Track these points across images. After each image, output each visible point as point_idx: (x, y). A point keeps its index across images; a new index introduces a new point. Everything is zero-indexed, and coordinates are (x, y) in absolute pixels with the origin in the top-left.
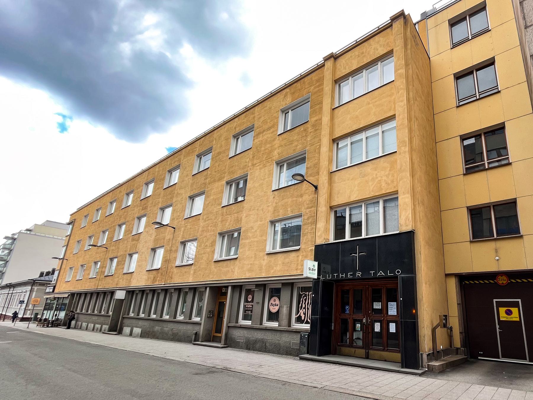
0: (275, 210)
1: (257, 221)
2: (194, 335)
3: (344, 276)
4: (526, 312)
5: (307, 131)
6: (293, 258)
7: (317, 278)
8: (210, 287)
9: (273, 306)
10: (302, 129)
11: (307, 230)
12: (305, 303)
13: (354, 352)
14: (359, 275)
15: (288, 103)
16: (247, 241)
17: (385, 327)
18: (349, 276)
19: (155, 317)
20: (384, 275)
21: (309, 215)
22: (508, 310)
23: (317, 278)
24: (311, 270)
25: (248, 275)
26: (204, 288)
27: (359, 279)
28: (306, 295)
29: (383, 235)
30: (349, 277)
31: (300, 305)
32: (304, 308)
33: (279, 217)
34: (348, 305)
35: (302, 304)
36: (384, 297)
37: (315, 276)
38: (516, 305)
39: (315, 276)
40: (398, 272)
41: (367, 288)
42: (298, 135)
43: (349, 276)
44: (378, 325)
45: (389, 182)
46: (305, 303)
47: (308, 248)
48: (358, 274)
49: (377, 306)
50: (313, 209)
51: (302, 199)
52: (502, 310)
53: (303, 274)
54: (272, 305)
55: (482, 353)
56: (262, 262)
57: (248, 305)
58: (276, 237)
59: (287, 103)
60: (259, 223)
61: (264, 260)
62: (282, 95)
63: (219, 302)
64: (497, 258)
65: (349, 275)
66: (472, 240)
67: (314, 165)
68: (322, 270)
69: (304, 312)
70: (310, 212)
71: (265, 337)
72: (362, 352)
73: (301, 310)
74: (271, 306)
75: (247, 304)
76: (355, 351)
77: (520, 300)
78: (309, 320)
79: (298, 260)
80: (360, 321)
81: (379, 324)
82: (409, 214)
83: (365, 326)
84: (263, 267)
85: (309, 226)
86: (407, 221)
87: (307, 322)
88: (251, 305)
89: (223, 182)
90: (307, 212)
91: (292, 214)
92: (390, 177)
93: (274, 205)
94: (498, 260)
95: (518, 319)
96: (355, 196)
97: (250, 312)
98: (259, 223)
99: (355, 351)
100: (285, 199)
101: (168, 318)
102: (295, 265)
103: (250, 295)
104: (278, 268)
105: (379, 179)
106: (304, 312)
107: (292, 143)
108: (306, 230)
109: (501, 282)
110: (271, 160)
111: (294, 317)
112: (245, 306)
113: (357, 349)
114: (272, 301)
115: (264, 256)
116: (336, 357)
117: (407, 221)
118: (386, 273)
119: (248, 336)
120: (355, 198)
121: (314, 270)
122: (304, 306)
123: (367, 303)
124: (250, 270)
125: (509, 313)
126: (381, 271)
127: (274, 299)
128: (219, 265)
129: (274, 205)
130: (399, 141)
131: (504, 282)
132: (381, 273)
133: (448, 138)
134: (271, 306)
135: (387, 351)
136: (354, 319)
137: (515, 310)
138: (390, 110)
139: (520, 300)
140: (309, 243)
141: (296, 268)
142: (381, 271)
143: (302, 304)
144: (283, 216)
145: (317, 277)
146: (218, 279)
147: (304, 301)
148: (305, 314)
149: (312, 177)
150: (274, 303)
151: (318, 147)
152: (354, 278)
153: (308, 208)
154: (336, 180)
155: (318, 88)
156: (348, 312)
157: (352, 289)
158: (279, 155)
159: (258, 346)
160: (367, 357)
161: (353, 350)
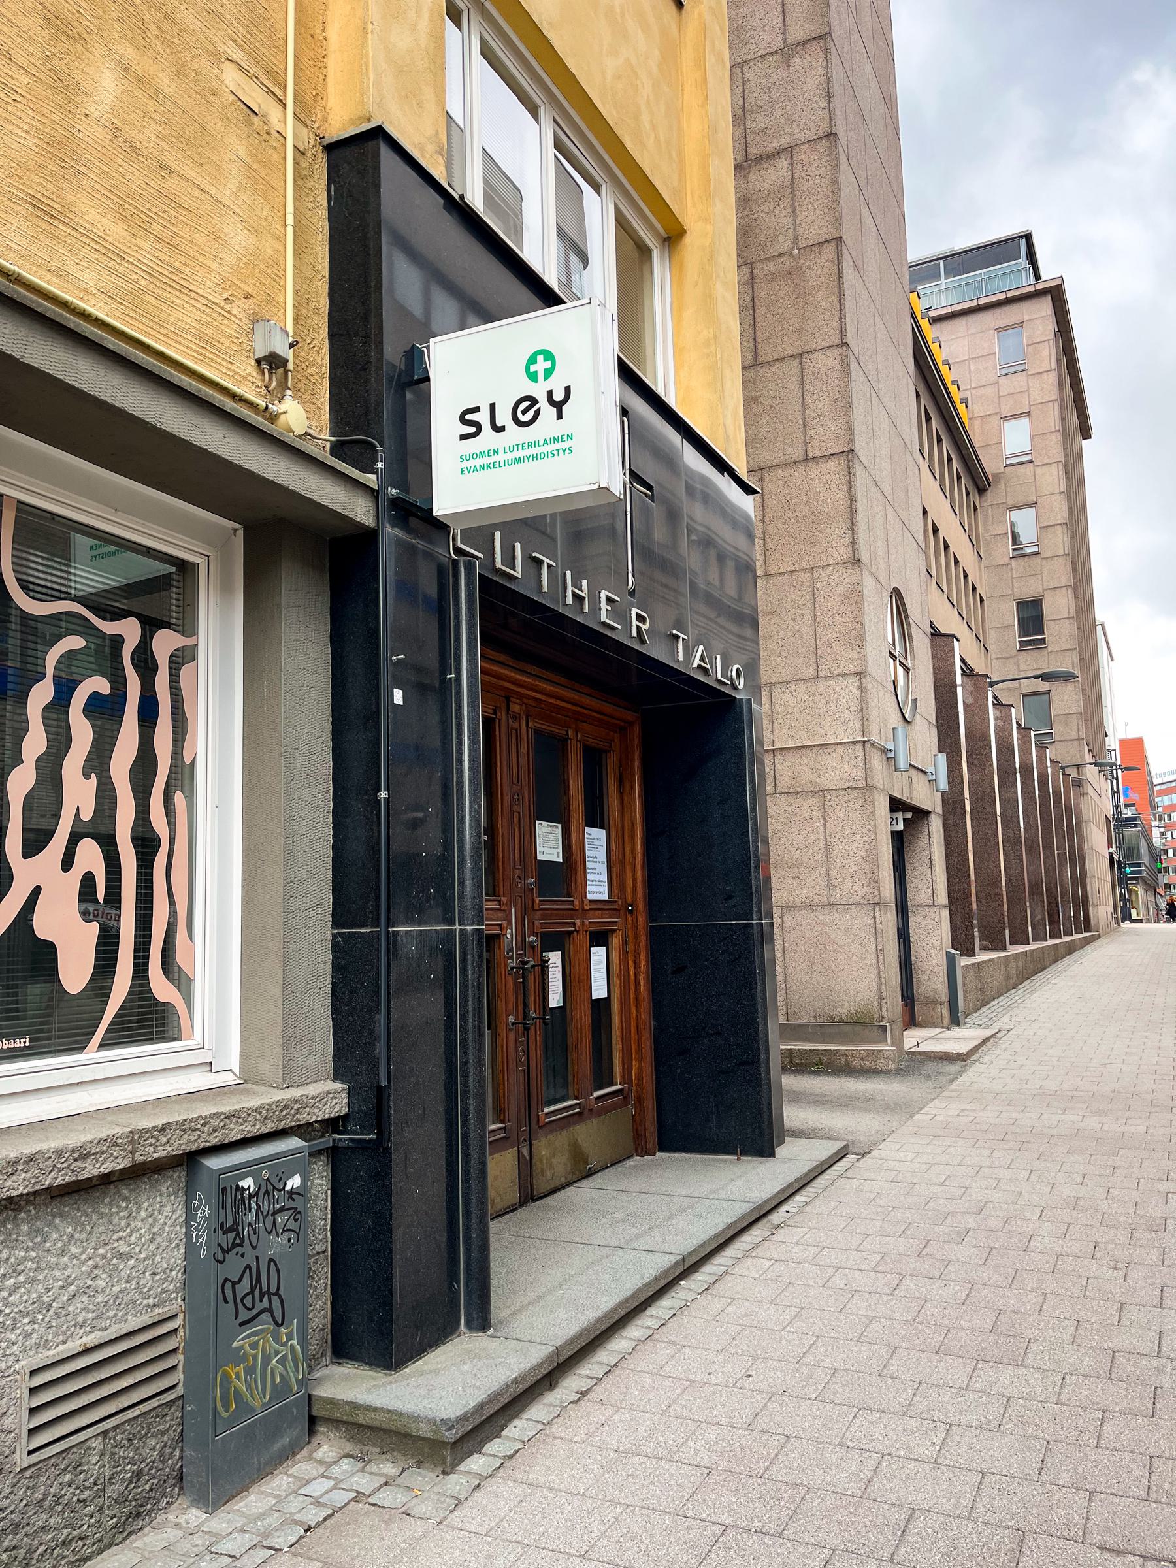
12: (98, 762)
46: (98, 762)
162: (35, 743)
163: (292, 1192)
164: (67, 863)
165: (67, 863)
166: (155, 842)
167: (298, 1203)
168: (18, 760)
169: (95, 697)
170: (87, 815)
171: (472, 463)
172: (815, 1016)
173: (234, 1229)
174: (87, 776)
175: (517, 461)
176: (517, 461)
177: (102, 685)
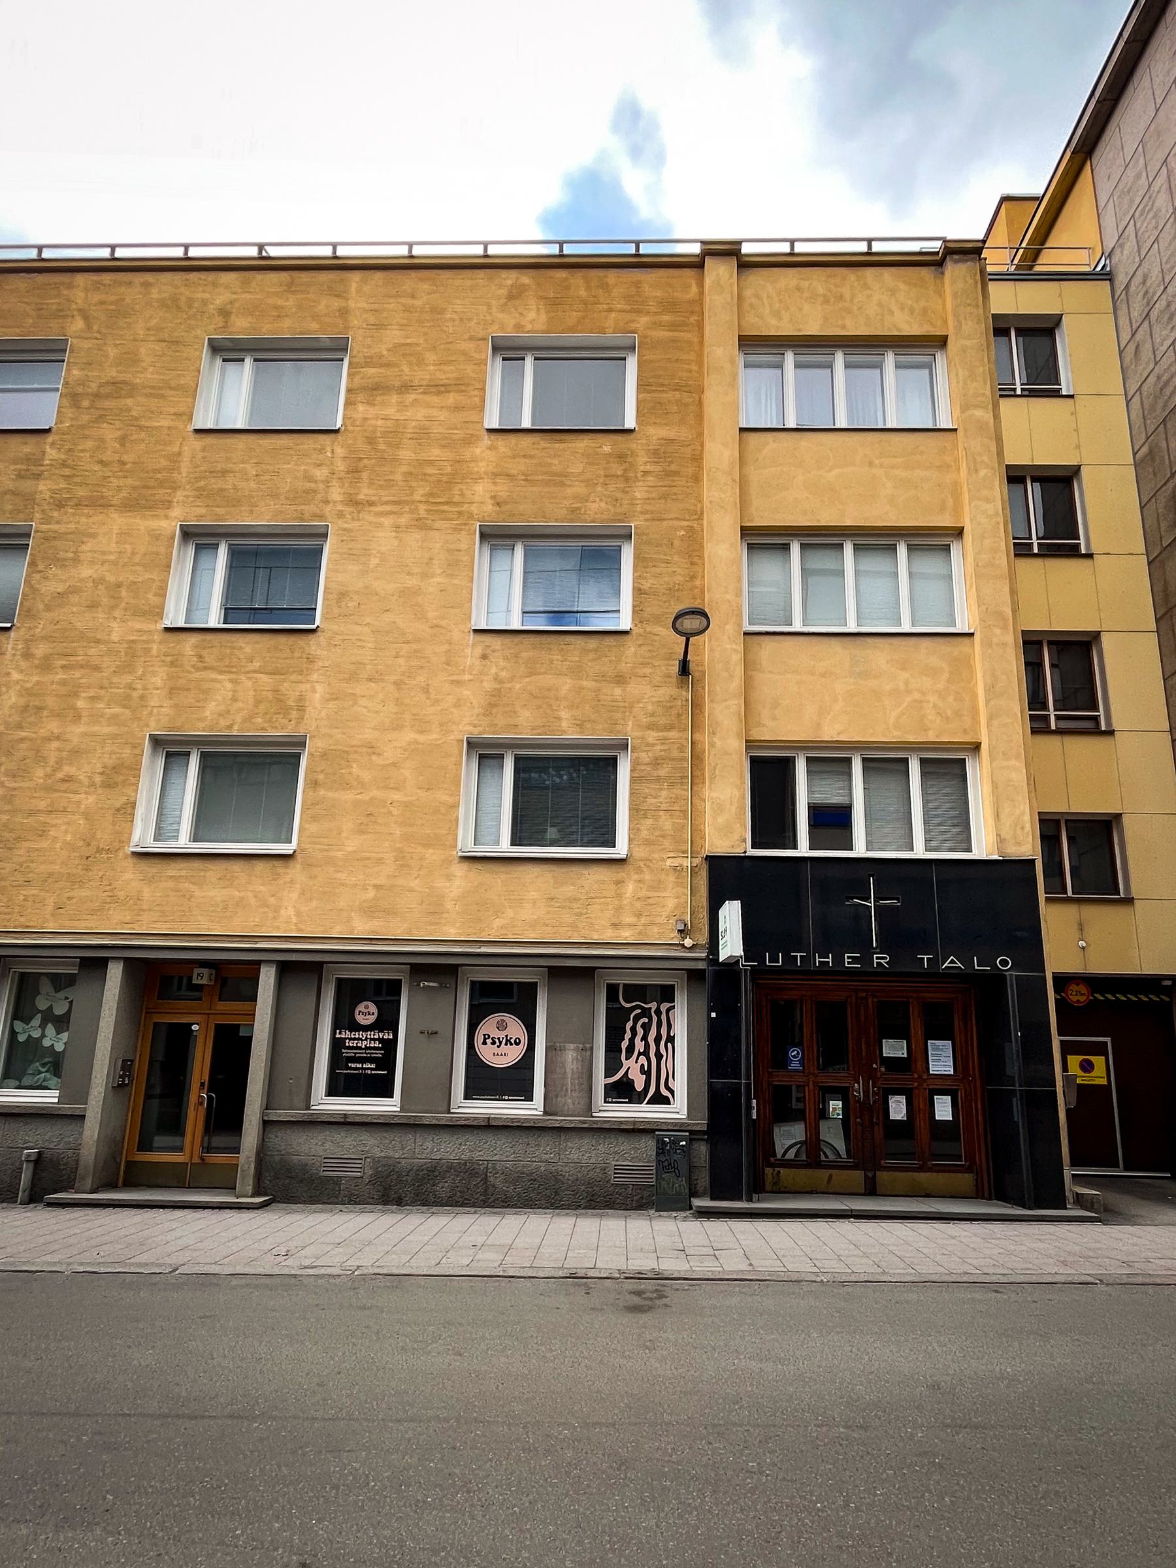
0: (495, 702)
1: (397, 727)
2: (31, 1165)
4: (1121, 1068)
5: (631, 465)
6: (595, 886)
8: (127, 961)
9: (493, 1043)
11: (653, 801)
12: (645, 1038)
13: (825, 1182)
15: (529, 327)
16: (348, 796)
17: (920, 1107)
18: (849, 963)
19: (56, 1100)
22: (1084, 1060)
25: (362, 927)
26: (73, 965)
27: (881, 973)
28: (646, 1013)
29: (806, 855)
32: (640, 1054)
33: (516, 733)
34: (800, 1044)
35: (632, 1041)
36: (916, 1026)
38: (1100, 1050)
40: (1004, 963)
42: (589, 464)
43: (849, 963)
44: (899, 1101)
45: (949, 713)
46: (645, 1038)
47: (664, 860)
48: (877, 958)
49: (894, 1049)
51: (624, 690)
52: (1074, 1061)
54: (489, 1041)
56: (441, 884)
57: (359, 1039)
58: (173, 793)
59: (523, 326)
60: (409, 736)
61: (449, 877)
62: (501, 286)
63: (155, 1024)
64: (1082, 943)
65: (846, 960)
70: (663, 740)
71: (478, 1155)
72: (858, 1176)
74: (484, 1043)
75: (346, 1034)
76: (831, 1176)
77: (1108, 1040)
79: (619, 896)
80: (843, 1093)
82: (1023, 814)
84: (449, 905)
86: (1019, 832)
88: (375, 1040)
89: (164, 524)
90: (650, 740)
91: (581, 733)
92: (951, 699)
93: (488, 685)
94: (1083, 948)
95: (1104, 1082)
96: (838, 727)
97: (373, 1066)
98: (409, 736)
99: (831, 1176)
100: (545, 673)
101: (56, 1100)
102: (609, 913)
103: (366, 1003)
104: (527, 913)
105: (917, 696)
106: (642, 1065)
107: (562, 484)
108: (651, 800)
109: (1074, 999)
111: (600, 1081)
112: (337, 1045)
113: (835, 1172)
114: (488, 1026)
115: (447, 862)
116: (117, 1192)
117: (1019, 832)
119: (390, 1153)
120: (839, 734)
122: (639, 1046)
124: (370, 911)
125: (1087, 1067)
128: (171, 873)
129: (485, 684)
130: (983, 608)
131: (1082, 999)
132: (951, 962)
134: (484, 1043)
135: (930, 1170)
136: (821, 1088)
137: (1098, 1061)
138: (943, 509)
139: (1108, 1040)
140: (667, 843)
141: (615, 920)
143: (632, 1041)
144: (535, 732)
146: (323, 933)
148: (648, 1074)
149: (662, 626)
150: (496, 1034)
151: (683, 532)
153: (651, 727)
154: (764, 663)
155: (671, 334)
156: (795, 1065)
159: (443, 1188)
160: (871, 1191)
161: (824, 1174)
162: (628, 1035)
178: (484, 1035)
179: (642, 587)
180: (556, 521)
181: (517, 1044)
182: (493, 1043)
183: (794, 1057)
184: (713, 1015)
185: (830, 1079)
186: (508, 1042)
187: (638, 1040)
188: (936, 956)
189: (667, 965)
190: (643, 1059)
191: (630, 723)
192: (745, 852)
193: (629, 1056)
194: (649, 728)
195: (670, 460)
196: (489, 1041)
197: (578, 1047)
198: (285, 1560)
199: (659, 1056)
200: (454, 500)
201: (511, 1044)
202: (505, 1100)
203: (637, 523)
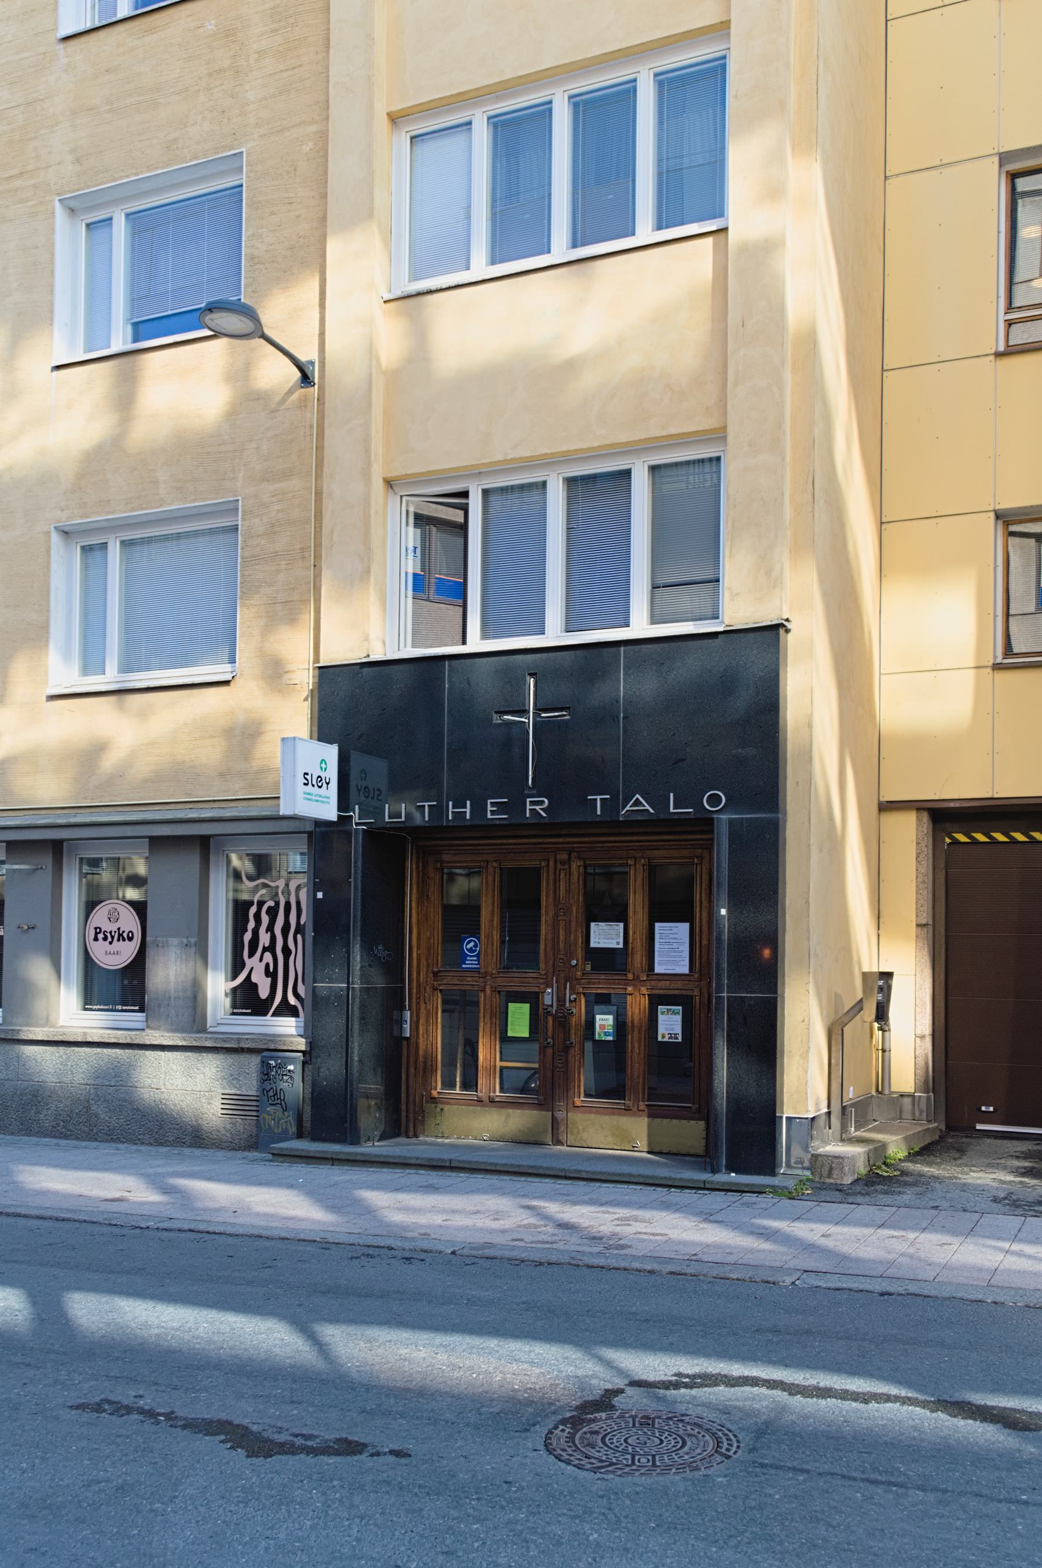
3: (468, 810)
7: (335, 818)
9: (105, 939)
10: (210, 27)
12: (270, 928)
14: (537, 808)
20: (652, 811)
21: (278, 511)
23: (335, 818)
24: (314, 783)
27: (539, 827)
30: (489, 816)
31: (248, 936)
32: (265, 949)
36: (637, 903)
37: (330, 812)
39: (330, 812)
41: (563, 863)
46: (270, 928)
50: (294, 484)
53: (279, 798)
54: (101, 936)
55: (983, 1108)
65: (489, 808)
66: (999, 660)
67: (291, 248)
68: (354, 782)
69: (267, 965)
73: (251, 955)
74: (96, 939)
78: (292, 1000)
80: (533, 999)
81: (526, 1008)
83: (550, 1019)
85: (278, 571)
87: (286, 1010)
106: (267, 965)
110: (35, 187)
118: (659, 801)
121: (325, 785)
122: (264, 939)
123: (562, 924)
126: (637, 796)
127: (111, 906)
133: (944, 162)
134: (96, 939)
142: (637, 796)
145: (339, 817)
147: (265, 919)
150: (108, 927)
152: (513, 821)
153: (268, 476)
156: (471, 963)
157: (491, 869)
158: (78, 160)
162: (251, 925)
163: (289, 1071)
164: (261, 960)
165: (261, 960)
166: (290, 952)
167: (292, 1074)
168: (246, 930)
169: (269, 908)
170: (267, 945)
171: (325, 800)
172: (140, 1066)
173: (267, 1074)
174: (267, 932)
175: (317, 801)
176: (317, 801)
177: (272, 903)
178: (96, 928)
179: (256, 253)
180: (149, 168)
181: (130, 939)
182: (105, 939)
183: (470, 950)
184: (320, 895)
185: (515, 981)
186: (121, 937)
187: (262, 930)
188: (615, 798)
189: (129, 831)
190: (268, 957)
191: (241, 474)
192: (368, 656)
193: (251, 955)
194: (264, 479)
195: (292, 20)
196: (101, 936)
197: (182, 942)
198: (561, 1427)
199: (286, 951)
200: (29, 168)
201: (124, 940)
202: (119, 1011)
203: (249, 146)
